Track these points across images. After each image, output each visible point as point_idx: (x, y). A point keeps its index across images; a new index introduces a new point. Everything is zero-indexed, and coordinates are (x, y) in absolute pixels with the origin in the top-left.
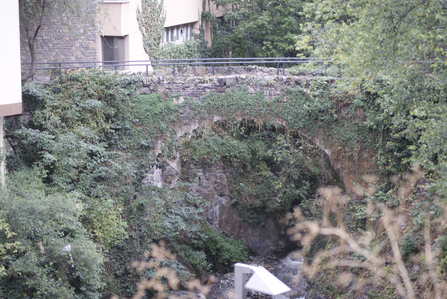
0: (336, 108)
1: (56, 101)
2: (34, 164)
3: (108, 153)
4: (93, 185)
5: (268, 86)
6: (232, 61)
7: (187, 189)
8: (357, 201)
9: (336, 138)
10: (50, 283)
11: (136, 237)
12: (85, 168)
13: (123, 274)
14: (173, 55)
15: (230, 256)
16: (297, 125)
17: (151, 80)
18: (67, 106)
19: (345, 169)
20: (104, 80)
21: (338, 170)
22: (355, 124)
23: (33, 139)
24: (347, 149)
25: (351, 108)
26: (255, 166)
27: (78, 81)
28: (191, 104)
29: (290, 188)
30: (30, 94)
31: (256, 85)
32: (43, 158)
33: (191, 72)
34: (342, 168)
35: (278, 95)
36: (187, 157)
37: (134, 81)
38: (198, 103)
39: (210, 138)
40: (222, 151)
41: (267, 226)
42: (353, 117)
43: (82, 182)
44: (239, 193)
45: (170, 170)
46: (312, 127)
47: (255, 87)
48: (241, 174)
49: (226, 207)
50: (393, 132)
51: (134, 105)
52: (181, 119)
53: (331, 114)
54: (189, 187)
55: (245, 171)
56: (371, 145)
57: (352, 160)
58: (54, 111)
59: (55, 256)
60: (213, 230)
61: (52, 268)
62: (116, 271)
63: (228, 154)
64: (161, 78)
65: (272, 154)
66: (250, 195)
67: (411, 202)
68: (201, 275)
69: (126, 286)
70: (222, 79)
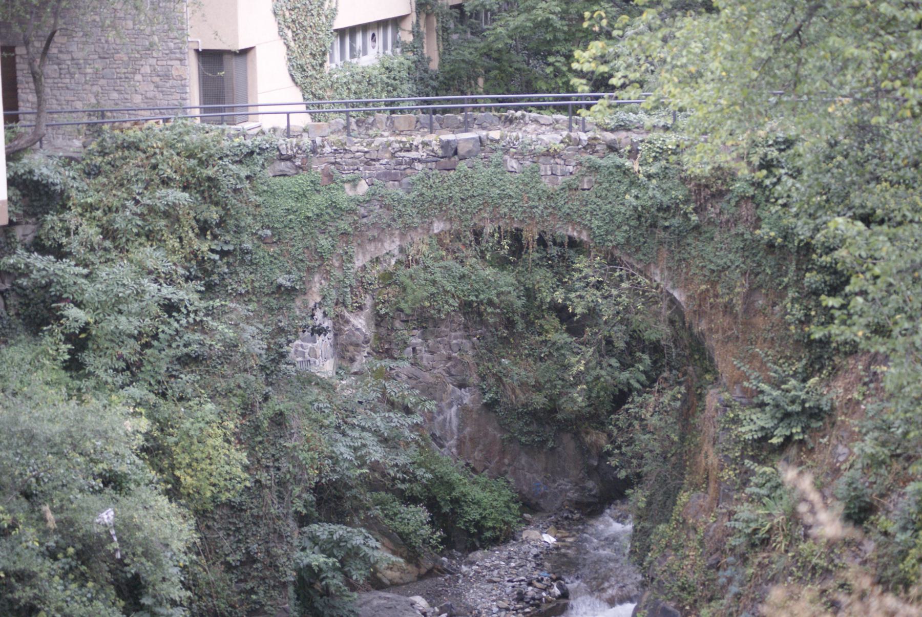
0: (696, 202)
1: (91, 193)
2: (43, 331)
3: (203, 304)
4: (174, 373)
5: (548, 155)
6: (485, 101)
7: (388, 375)
8: (744, 400)
9: (697, 267)
10: (68, 592)
11: (268, 482)
12: (155, 337)
13: (243, 563)
14: (353, 87)
15: (481, 514)
17: (297, 145)
18: (116, 203)
19: (717, 332)
20: (196, 148)
21: (702, 333)
22: (737, 234)
23: (43, 277)
24: (720, 290)
25: (729, 202)
26: (533, 323)
27: (138, 149)
28: (382, 196)
29: (609, 369)
30: (35, 178)
31: (522, 154)
32: (62, 316)
33: (384, 127)
34: (710, 330)
35: (571, 173)
36: (387, 304)
37: (260, 149)
38: (398, 194)
39: (436, 264)
40: (463, 291)
41: (560, 449)
42: (732, 220)
43: (149, 368)
44: (499, 380)
45: (351, 334)
46: (645, 242)
47: (520, 157)
48: (504, 341)
49: (471, 411)
50: (819, 251)
51: (259, 200)
52: (363, 228)
53: (686, 214)
54: (391, 369)
55: (512, 334)
56: (772, 280)
57: (731, 313)
59: (79, 534)
60: (445, 459)
61: (73, 560)
62: (227, 555)
63: (474, 299)
64: (318, 140)
65: (564, 300)
66: (522, 385)
67: (858, 403)
68: (419, 555)
69: (248, 587)
70: (448, 142)
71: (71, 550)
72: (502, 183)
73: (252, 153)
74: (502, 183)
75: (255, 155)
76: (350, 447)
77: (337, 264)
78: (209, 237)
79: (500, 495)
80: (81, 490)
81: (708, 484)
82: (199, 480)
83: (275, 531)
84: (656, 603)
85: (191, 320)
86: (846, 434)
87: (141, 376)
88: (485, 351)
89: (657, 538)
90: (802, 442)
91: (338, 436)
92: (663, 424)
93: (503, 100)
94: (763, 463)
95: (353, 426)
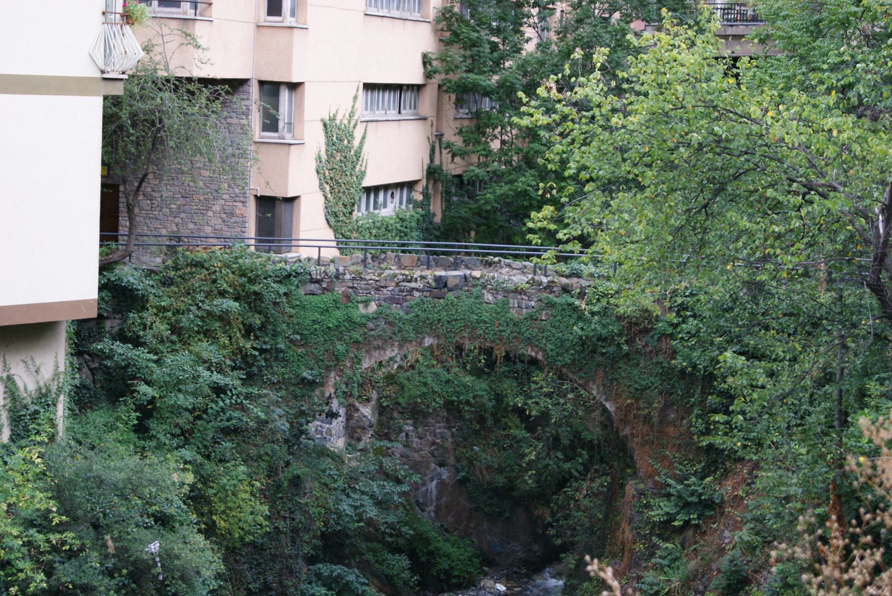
0: (627, 335)
3: (244, 390)
8: (654, 491)
12: (205, 412)
13: (261, 590)
14: (374, 232)
16: (561, 359)
18: (183, 307)
19: (637, 437)
20: (247, 269)
21: (626, 437)
22: (657, 363)
23: (123, 360)
24: (641, 404)
25: (652, 337)
26: (500, 421)
27: (203, 267)
31: (496, 290)
32: (135, 391)
34: (632, 435)
39: (428, 371)
43: (198, 435)
44: (470, 462)
48: (477, 433)
51: (293, 311)
52: (371, 339)
53: (619, 344)
54: (388, 448)
57: (649, 422)
58: (161, 315)
62: (250, 583)
63: (455, 399)
64: (341, 269)
66: (489, 467)
67: (742, 499)
70: (440, 277)
71: (125, 571)
72: (479, 311)
74: (479, 311)
75: (292, 278)
76: (352, 506)
77: (349, 365)
78: (252, 338)
79: (466, 551)
80: (137, 525)
81: (623, 554)
82: (230, 524)
83: (287, 567)
85: (233, 402)
86: (731, 522)
87: (192, 441)
90: (697, 526)
91: (344, 497)
92: (592, 505)
93: (489, 248)
94: (666, 540)
95: (354, 490)
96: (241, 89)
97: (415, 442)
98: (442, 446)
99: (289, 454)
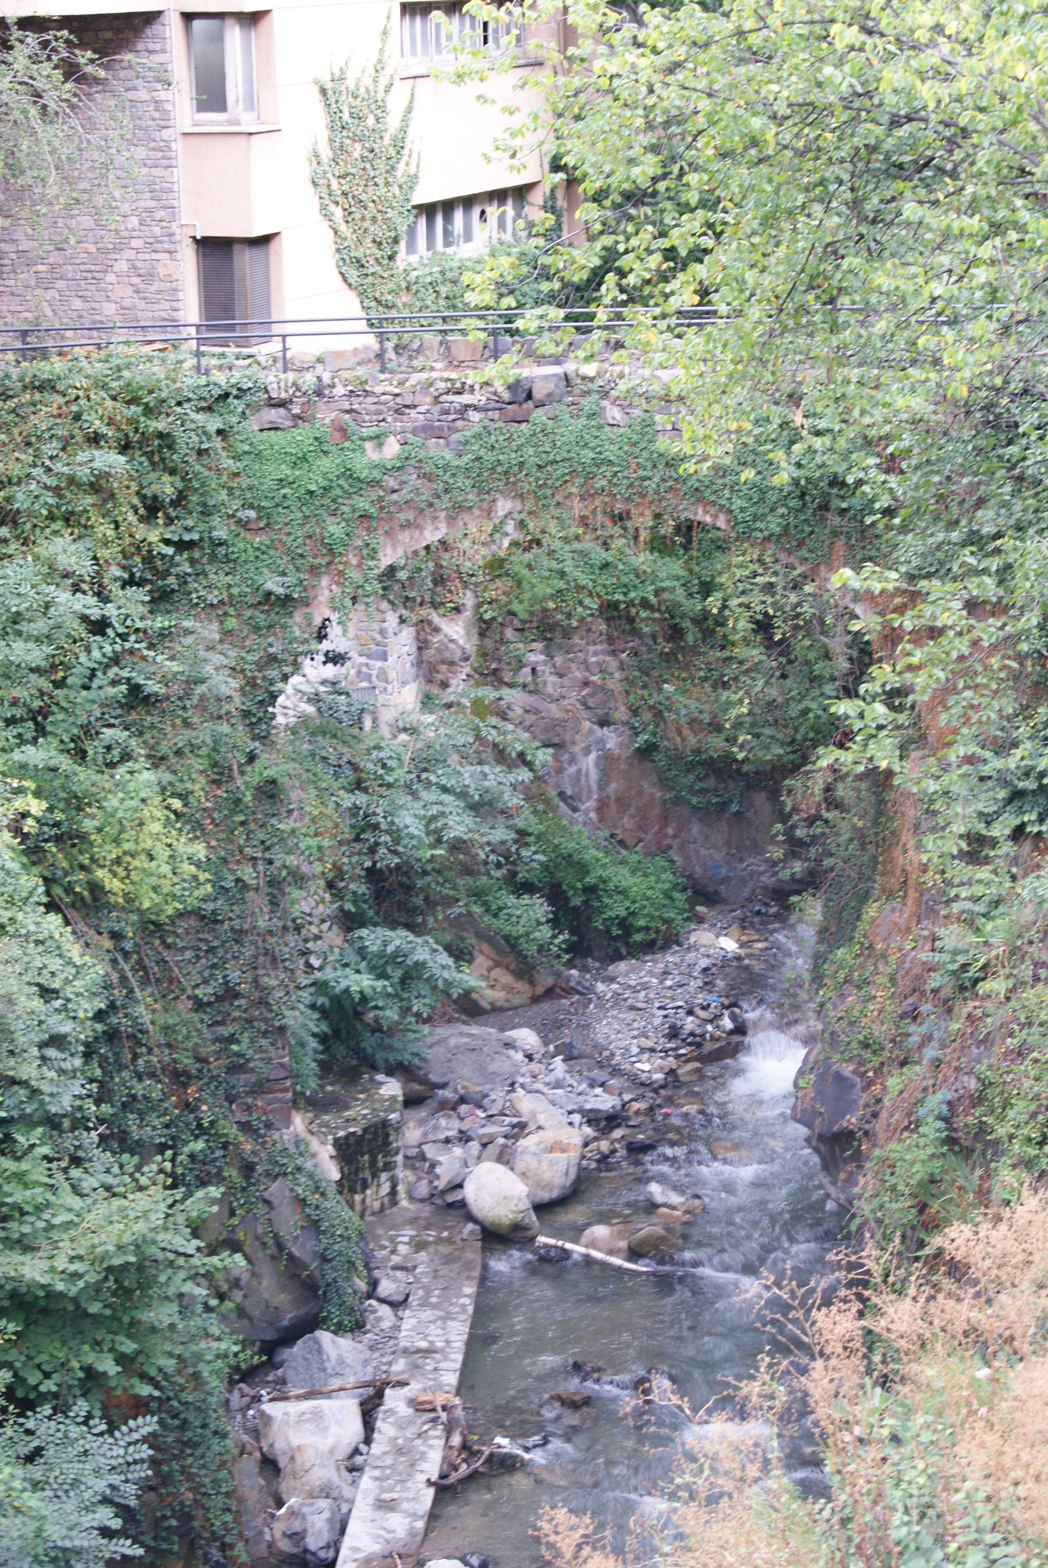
13: (220, 999)
20: (141, 388)
26: (713, 632)
39: (567, 548)
41: (749, 814)
44: (659, 714)
45: (442, 648)
48: (669, 658)
63: (621, 598)
64: (326, 378)
66: (692, 722)
69: (226, 1034)
73: (227, 395)
75: (230, 399)
84: (827, 1062)
87: (49, 728)
88: (637, 673)
89: (834, 968)
95: (429, 784)
96: (148, 32)
97: (551, 682)
98: (602, 688)
99: (253, 739)
